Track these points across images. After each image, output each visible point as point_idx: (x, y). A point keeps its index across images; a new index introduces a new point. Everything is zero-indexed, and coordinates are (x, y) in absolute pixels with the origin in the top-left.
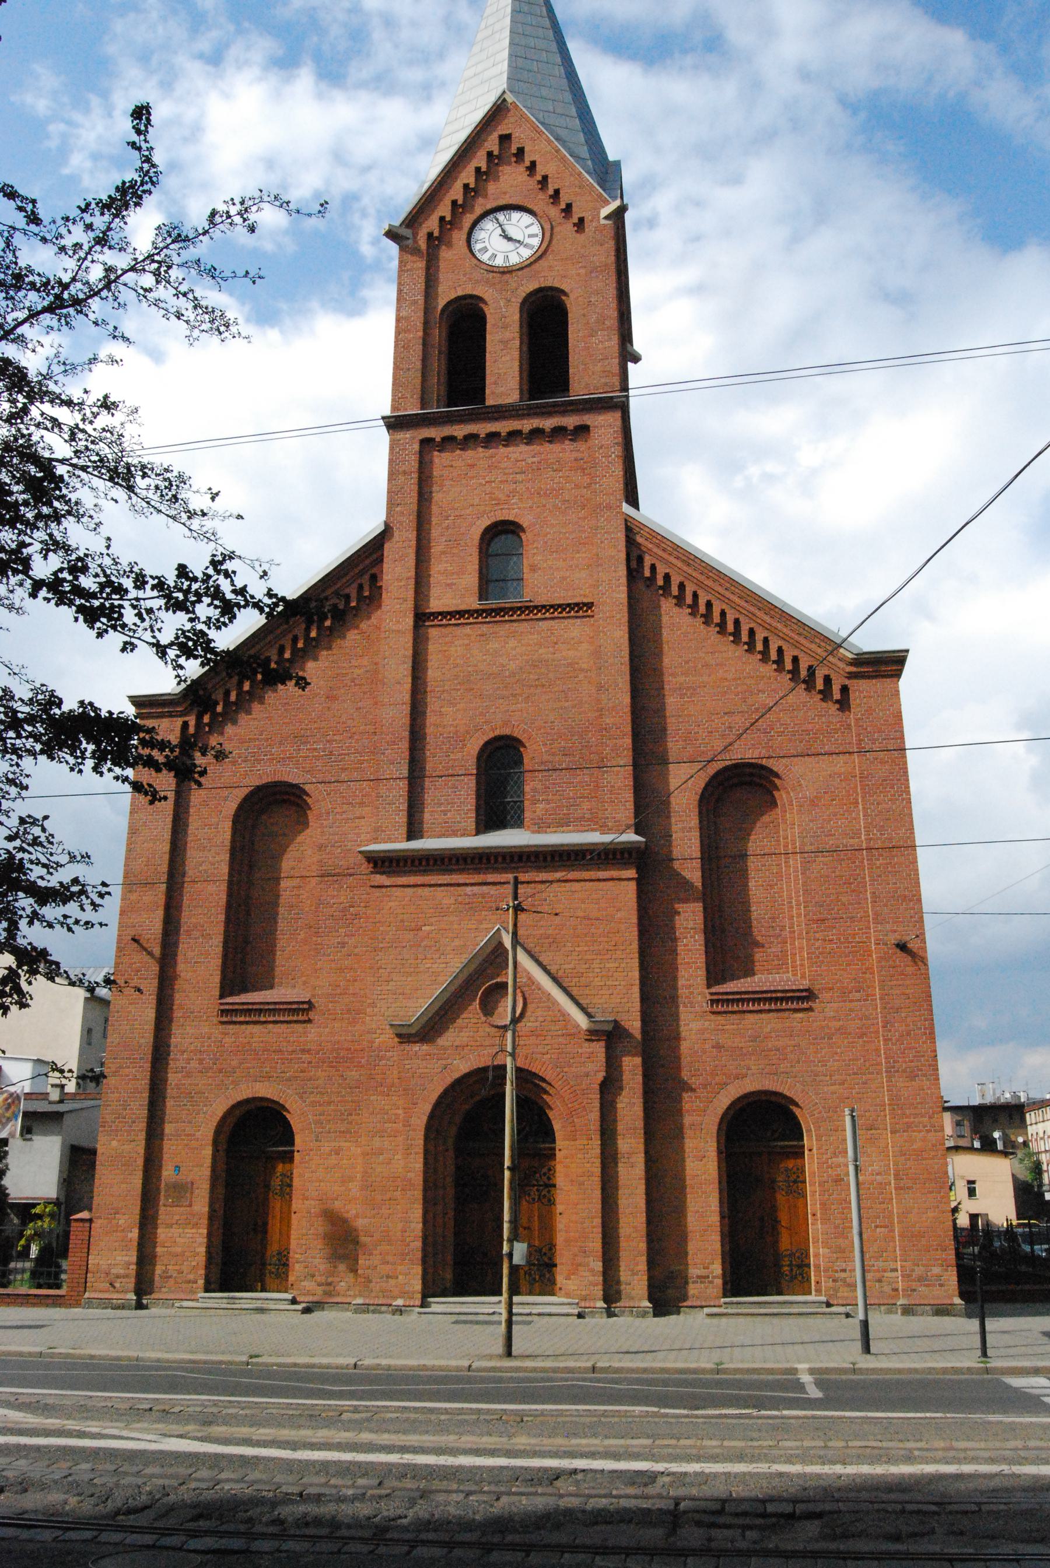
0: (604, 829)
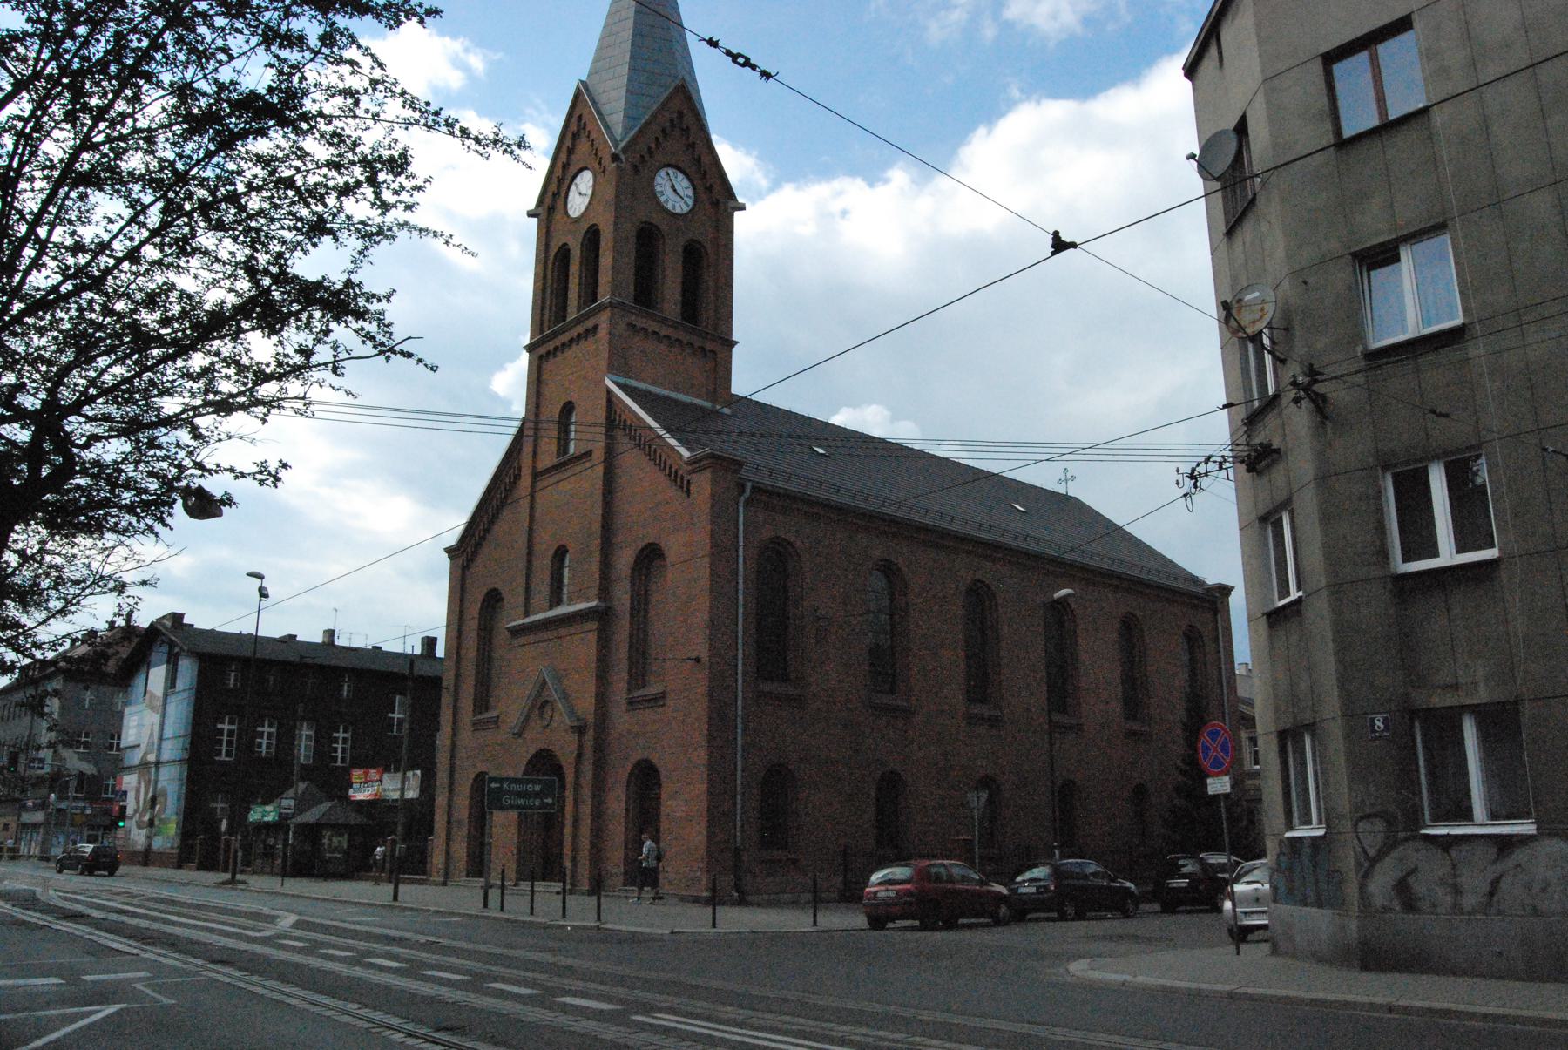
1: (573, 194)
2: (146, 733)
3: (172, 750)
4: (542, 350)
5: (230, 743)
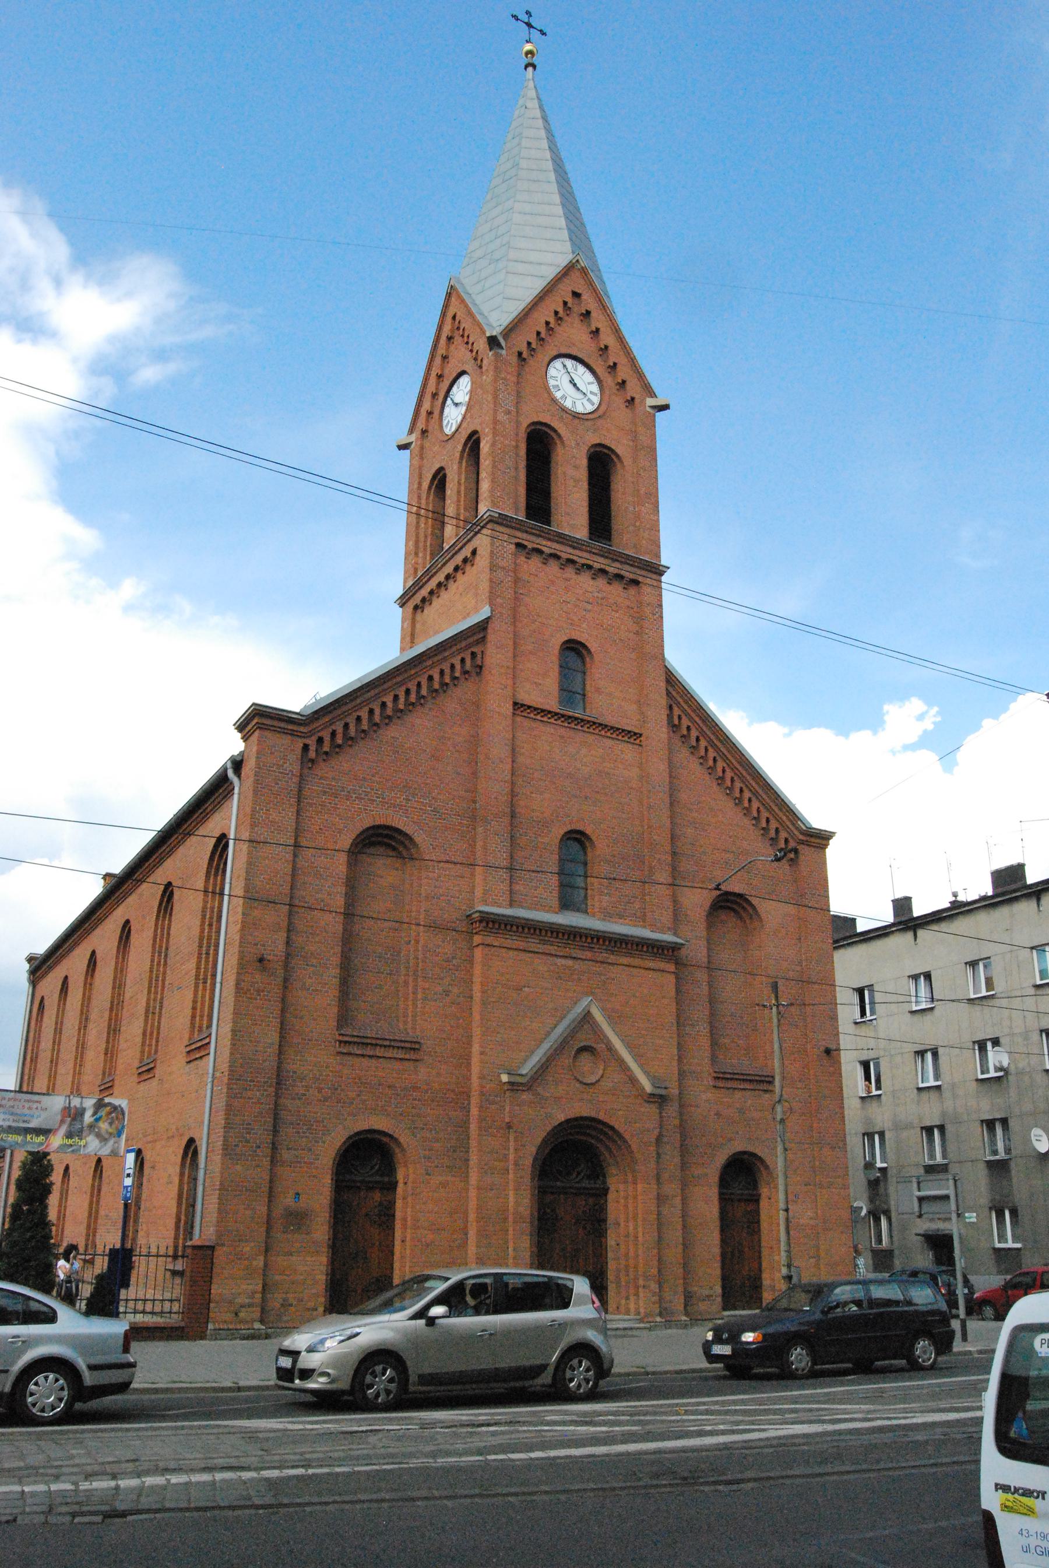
0: (653, 927)
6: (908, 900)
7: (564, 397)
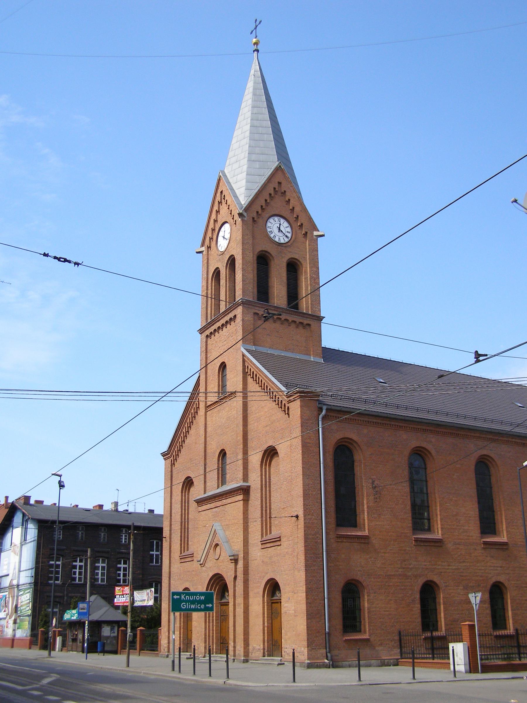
1: (220, 239)
2: (12, 568)
3: (26, 578)
4: (208, 332)
5: (103, 574)
6: (103, 505)
7: (275, 236)
